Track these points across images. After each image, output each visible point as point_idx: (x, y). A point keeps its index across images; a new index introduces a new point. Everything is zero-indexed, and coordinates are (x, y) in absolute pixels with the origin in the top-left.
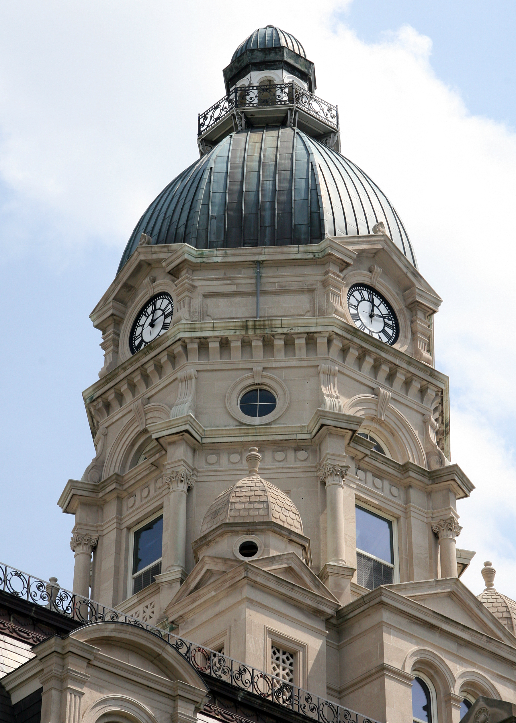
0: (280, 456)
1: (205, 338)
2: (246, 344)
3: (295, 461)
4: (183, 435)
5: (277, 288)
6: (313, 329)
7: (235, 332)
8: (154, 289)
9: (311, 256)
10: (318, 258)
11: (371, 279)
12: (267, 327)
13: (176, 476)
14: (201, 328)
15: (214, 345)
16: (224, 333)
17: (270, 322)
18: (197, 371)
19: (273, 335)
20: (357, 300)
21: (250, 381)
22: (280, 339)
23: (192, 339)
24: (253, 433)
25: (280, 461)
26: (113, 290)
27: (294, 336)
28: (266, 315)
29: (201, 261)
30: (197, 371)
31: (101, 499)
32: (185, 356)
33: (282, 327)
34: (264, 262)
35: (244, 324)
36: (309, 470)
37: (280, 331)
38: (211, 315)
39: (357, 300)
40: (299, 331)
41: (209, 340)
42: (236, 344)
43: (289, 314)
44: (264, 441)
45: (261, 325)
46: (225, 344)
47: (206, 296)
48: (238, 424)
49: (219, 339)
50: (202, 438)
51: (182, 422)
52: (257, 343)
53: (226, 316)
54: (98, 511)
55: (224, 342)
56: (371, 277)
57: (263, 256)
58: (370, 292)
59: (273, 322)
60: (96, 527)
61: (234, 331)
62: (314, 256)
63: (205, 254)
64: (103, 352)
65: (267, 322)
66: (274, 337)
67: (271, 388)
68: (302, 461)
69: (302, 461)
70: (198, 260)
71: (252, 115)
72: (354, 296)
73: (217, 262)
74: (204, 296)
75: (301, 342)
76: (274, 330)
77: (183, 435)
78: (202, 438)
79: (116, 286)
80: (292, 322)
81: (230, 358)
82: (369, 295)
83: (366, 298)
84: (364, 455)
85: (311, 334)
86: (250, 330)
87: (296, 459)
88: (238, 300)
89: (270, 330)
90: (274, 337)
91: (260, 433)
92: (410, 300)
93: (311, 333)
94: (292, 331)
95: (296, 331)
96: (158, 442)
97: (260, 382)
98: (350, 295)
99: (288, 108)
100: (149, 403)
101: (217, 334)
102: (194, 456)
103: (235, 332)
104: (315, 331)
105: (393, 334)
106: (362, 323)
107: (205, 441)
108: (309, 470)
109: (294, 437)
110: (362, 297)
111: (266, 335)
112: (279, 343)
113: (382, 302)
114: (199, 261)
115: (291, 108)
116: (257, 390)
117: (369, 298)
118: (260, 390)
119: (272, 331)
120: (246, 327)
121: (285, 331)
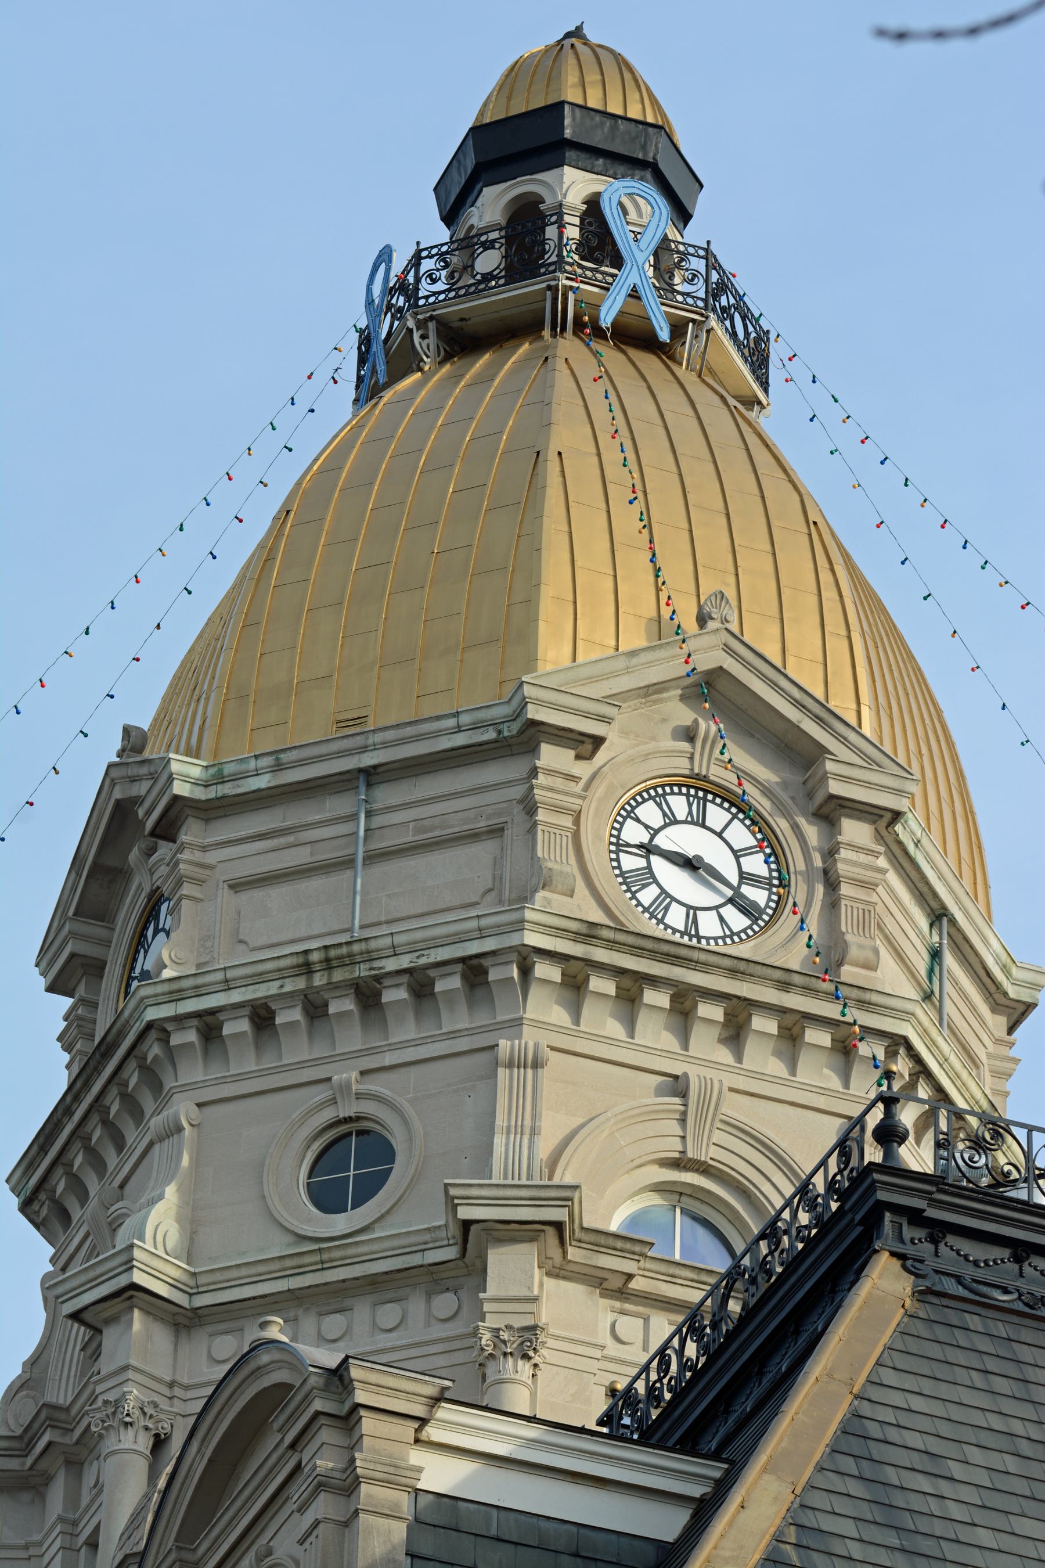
0: (388, 1315)
1: (212, 1012)
2: (315, 1010)
3: (428, 1325)
4: (131, 1297)
5: (410, 839)
6: (474, 948)
7: (282, 986)
8: (152, 874)
9: (490, 735)
10: (511, 737)
11: (691, 758)
12: (358, 959)
13: (114, 1413)
14: (197, 987)
15: (237, 1026)
16: (254, 991)
17: (363, 946)
18: (199, 1105)
19: (378, 979)
20: (647, 827)
21: (328, 1115)
22: (397, 986)
23: (180, 1020)
24: (316, 1263)
25: (390, 1331)
26: (74, 889)
27: (432, 973)
28: (383, 919)
29: (220, 794)
30: (199, 1105)
31: (34, 1473)
32: (170, 1069)
33: (395, 955)
34: (380, 770)
35: (301, 960)
36: (457, 1345)
37: (391, 965)
38: (246, 939)
39: (647, 827)
40: (439, 959)
41: (222, 1016)
42: (289, 1016)
43: (441, 905)
44: (344, 1281)
45: (342, 957)
46: (262, 1017)
47: (237, 886)
48: (291, 1239)
49: (247, 1011)
50: (191, 1295)
51: (121, 1265)
52: (343, 1005)
53: (283, 938)
54: (33, 1501)
55: (263, 1012)
56: (693, 754)
57: (370, 754)
58: (696, 796)
59: (373, 945)
60: (26, 1547)
61: (278, 983)
62: (500, 732)
63: (226, 772)
64: (66, 1057)
65: (356, 948)
66: (380, 983)
67: (378, 1123)
68: (445, 1320)
69: (445, 1320)
70: (212, 793)
71: (462, 320)
72: (638, 820)
73: (259, 790)
74: (231, 887)
75: (450, 983)
76: (376, 964)
77: (131, 1297)
78: (191, 1295)
79: (79, 875)
80: (419, 935)
81: (280, 1058)
82: (690, 805)
83: (681, 815)
84: (625, 1277)
85: (475, 962)
86: (318, 974)
87: (430, 1318)
88: (317, 883)
89: (367, 965)
90: (380, 983)
91: (331, 1261)
92: (820, 797)
93: (471, 957)
94: (423, 961)
95: (432, 960)
96: (82, 1322)
97: (352, 1115)
98: (625, 818)
99: (544, 285)
100: (121, 1198)
101: (236, 996)
102: (176, 1345)
103: (282, 986)
104: (479, 951)
105: (769, 900)
106: (663, 891)
107: (201, 1301)
108: (457, 1345)
109: (416, 1260)
110: (665, 815)
111: (361, 981)
112: (395, 995)
113: (735, 816)
114: (212, 795)
115: (553, 283)
116: (350, 1134)
117: (690, 813)
118: (360, 1133)
119: (371, 969)
120: (306, 968)
121: (404, 962)
